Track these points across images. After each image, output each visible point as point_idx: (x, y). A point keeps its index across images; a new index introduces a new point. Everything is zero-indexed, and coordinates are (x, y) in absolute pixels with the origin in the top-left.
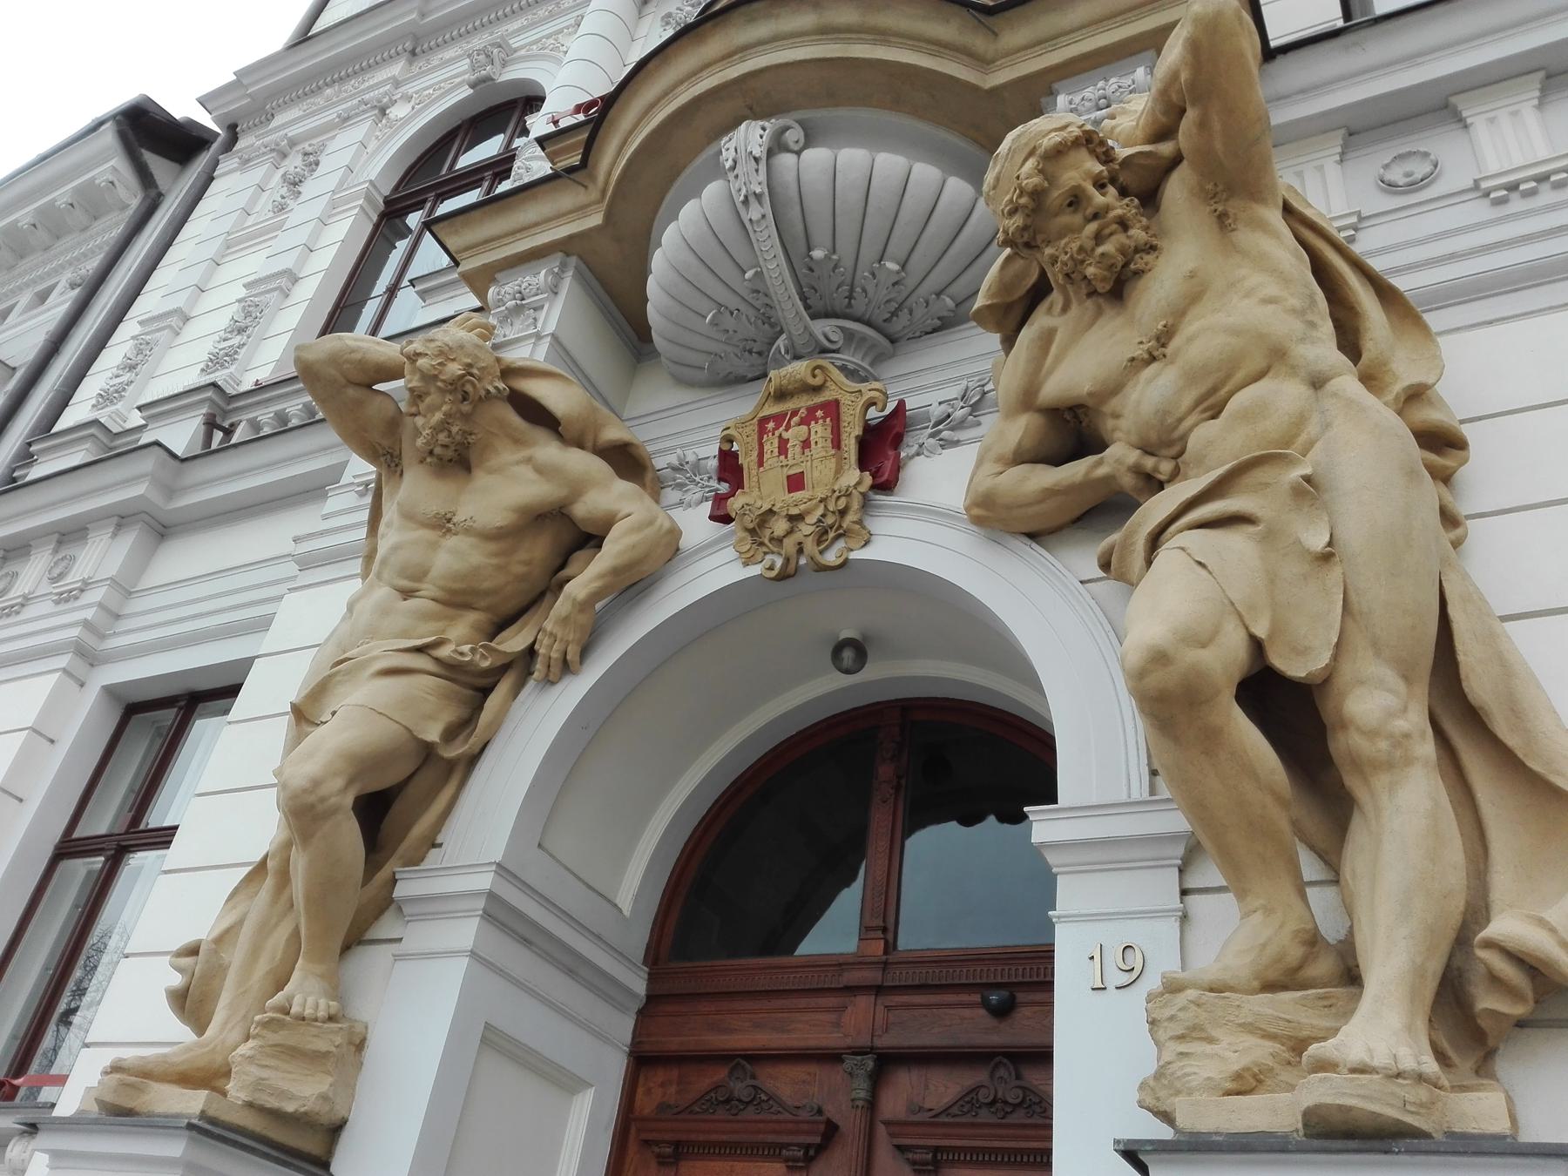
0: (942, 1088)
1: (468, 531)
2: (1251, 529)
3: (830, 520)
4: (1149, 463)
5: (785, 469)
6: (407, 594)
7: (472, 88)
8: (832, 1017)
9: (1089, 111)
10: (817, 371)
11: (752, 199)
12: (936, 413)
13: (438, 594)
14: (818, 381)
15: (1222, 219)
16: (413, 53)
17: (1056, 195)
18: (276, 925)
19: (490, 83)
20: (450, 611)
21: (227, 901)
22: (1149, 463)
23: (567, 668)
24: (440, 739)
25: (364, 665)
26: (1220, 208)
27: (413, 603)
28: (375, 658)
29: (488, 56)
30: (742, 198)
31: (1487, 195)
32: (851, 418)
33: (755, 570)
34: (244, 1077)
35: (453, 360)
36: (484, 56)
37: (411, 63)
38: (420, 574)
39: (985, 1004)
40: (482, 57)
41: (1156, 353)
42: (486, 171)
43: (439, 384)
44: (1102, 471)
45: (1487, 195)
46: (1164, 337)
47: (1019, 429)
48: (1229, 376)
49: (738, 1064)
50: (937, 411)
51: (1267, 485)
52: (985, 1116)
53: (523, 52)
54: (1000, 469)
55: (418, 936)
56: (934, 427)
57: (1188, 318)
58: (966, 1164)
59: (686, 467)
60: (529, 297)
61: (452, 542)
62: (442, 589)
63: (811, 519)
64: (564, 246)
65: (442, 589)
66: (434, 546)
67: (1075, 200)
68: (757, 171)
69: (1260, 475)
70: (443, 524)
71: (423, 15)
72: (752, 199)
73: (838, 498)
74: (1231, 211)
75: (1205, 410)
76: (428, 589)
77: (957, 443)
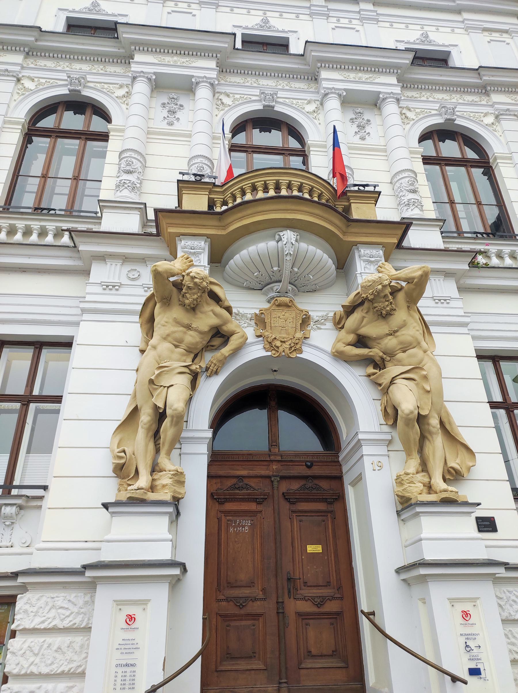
0: (295, 486)
1: (196, 330)
2: (414, 382)
3: (292, 345)
4: (385, 356)
5: (281, 328)
6: (176, 346)
7: (69, 91)
8: (266, 467)
9: (368, 257)
10: (291, 302)
11: (289, 254)
12: (316, 319)
13: (186, 348)
14: (290, 304)
15: (408, 307)
16: (28, 53)
17: (382, 294)
18: (148, 444)
19: (79, 93)
20: (188, 353)
21: (113, 434)
22: (385, 356)
23: (216, 373)
24: (265, 409)
25: (173, 369)
26: (409, 305)
27: (178, 350)
28: (176, 368)
29: (79, 82)
30: (286, 253)
31: (435, 300)
32: (299, 318)
33: (269, 354)
34: (171, 489)
35: (204, 281)
36: (78, 81)
37: (25, 58)
38: (181, 341)
39: (306, 465)
40: (77, 81)
41: (392, 334)
42: (83, 135)
43: (200, 288)
44: (371, 354)
45: (435, 300)
46: (395, 332)
47: (351, 338)
48: (410, 346)
49: (241, 478)
50: (316, 319)
51: (417, 373)
52: (306, 491)
53: (91, 85)
54: (345, 346)
55: (187, 448)
56: (314, 323)
57: (402, 329)
58: (303, 502)
59: (240, 314)
60: (196, 249)
61: (191, 333)
62: (188, 347)
63: (288, 343)
64: (208, 236)
65: (188, 347)
66: (185, 333)
67: (385, 296)
68: (292, 247)
69: (416, 370)
70: (189, 327)
71: (36, 40)
72: (289, 254)
73: (296, 340)
74: (411, 306)
75: (402, 351)
76: (183, 346)
77: (321, 329)
